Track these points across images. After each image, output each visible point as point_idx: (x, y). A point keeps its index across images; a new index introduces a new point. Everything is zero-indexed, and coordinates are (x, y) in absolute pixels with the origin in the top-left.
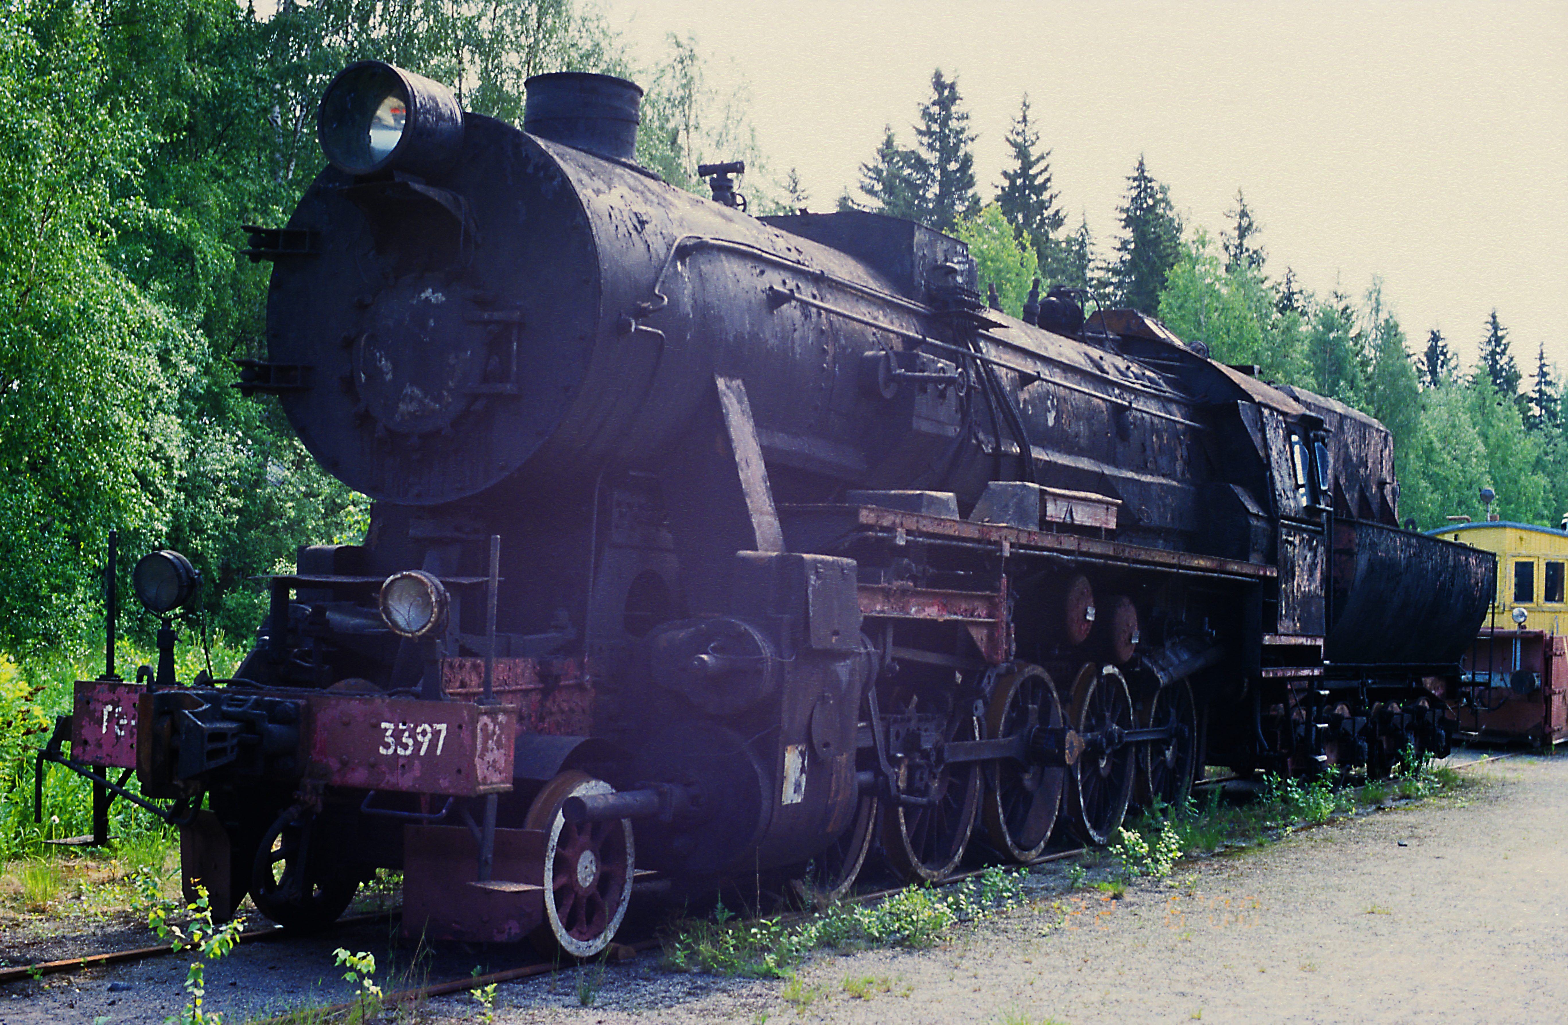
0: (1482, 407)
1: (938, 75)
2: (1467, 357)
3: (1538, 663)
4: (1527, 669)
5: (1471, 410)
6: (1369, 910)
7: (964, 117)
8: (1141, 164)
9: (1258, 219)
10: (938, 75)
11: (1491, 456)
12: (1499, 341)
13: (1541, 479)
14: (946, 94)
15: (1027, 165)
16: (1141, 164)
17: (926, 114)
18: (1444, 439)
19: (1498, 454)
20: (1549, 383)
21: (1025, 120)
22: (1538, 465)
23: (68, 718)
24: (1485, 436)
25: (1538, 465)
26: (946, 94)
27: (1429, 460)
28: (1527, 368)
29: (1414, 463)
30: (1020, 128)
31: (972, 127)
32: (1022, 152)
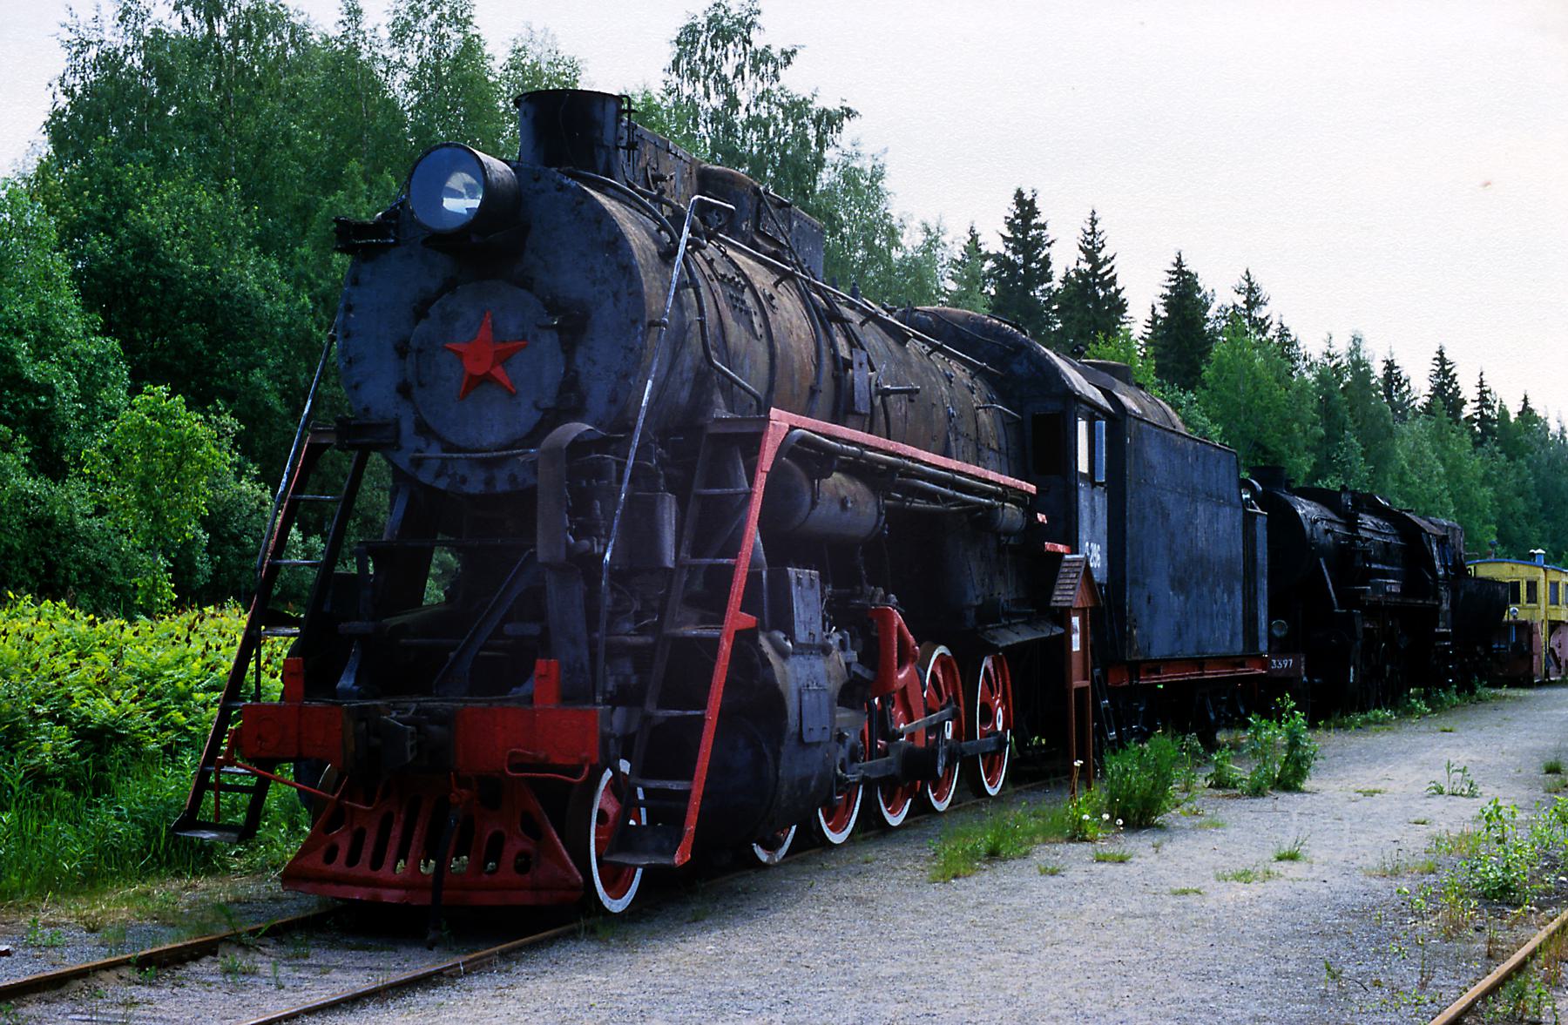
0: (1440, 433)
1: (1019, 194)
2: (1420, 387)
3: (1525, 637)
4: (1519, 641)
5: (1431, 438)
6: (1286, 849)
7: (1043, 227)
8: (1179, 260)
9: (1264, 293)
10: (1019, 194)
11: (1448, 475)
12: (1445, 373)
13: (1488, 491)
14: (1026, 208)
15: (1096, 265)
16: (1179, 260)
17: (1011, 225)
18: (1411, 463)
19: (1454, 473)
20: (1490, 407)
21: (1093, 232)
22: (1486, 480)
23: (238, 598)
24: (1443, 460)
25: (1486, 480)
26: (1026, 208)
27: (1401, 481)
28: (1469, 392)
29: (1392, 485)
30: (1090, 238)
31: (1050, 233)
32: (1091, 256)
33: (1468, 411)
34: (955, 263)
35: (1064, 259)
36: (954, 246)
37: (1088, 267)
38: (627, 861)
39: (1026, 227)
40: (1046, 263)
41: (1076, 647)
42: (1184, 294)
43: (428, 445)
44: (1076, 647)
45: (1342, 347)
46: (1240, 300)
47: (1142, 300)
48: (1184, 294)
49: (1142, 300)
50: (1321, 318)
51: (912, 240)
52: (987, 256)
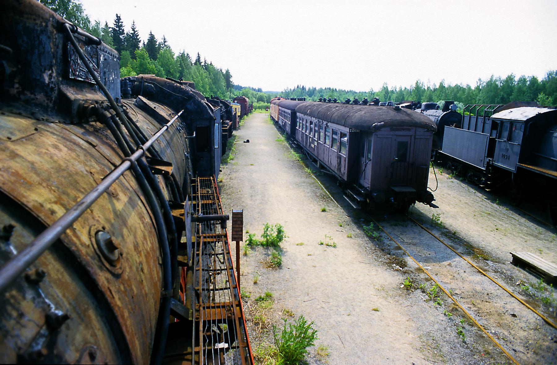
14: (119, 18)
31: (123, 24)
33: (203, 64)
34: (102, 28)
35: (127, 29)
36: (102, 26)
37: (133, 32)
38: (173, 221)
39: (119, 22)
40: (123, 30)
41: (181, 112)
42: (152, 39)
43: (99, 329)
44: (181, 112)
45: (414, 86)
46: (163, 41)
47: (144, 38)
48: (152, 39)
49: (144, 38)
50: (178, 45)
51: (93, 24)
52: (110, 28)
